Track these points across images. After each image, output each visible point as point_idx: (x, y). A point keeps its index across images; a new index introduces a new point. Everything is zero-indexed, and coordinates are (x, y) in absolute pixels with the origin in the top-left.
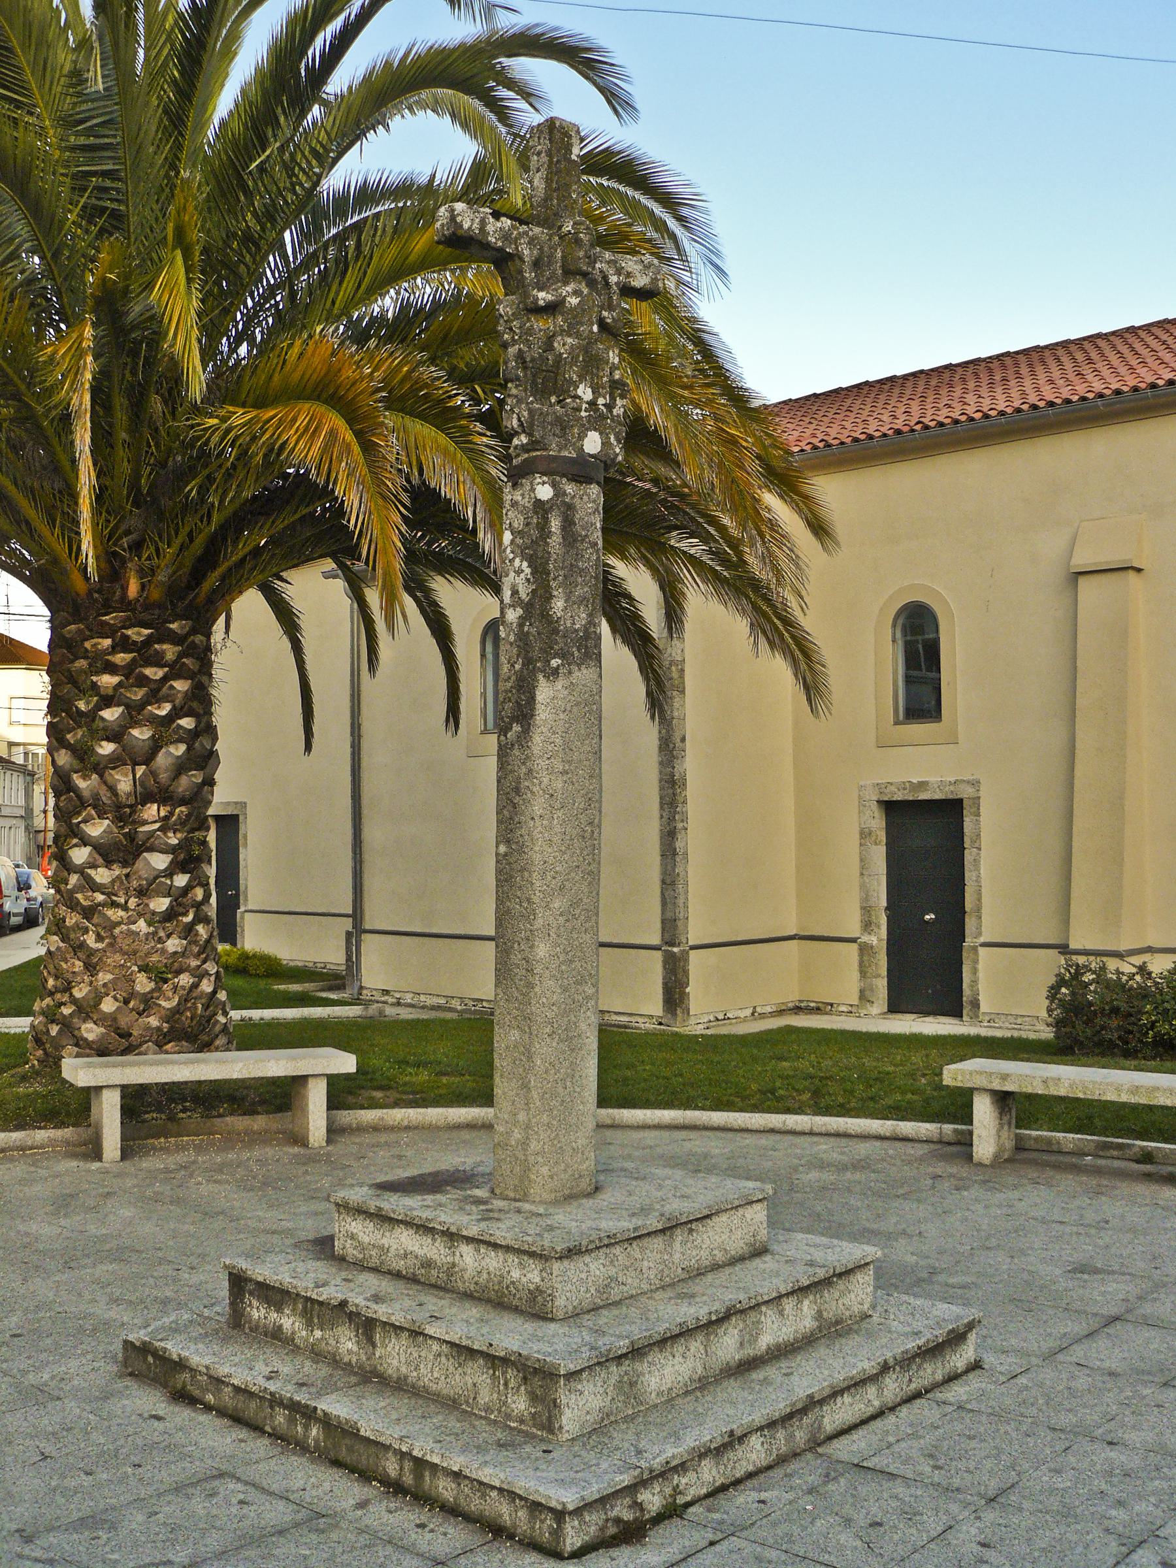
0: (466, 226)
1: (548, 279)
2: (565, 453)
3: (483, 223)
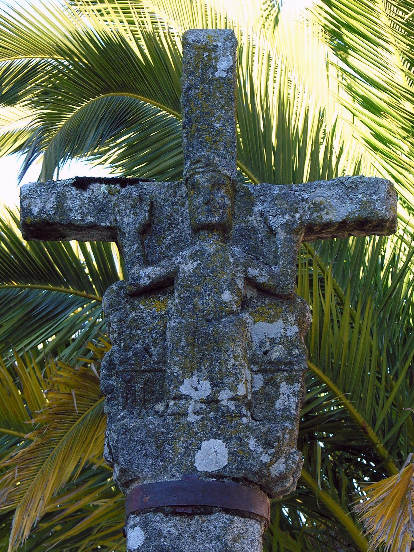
0: (35, 210)
1: (169, 248)
2: (167, 478)
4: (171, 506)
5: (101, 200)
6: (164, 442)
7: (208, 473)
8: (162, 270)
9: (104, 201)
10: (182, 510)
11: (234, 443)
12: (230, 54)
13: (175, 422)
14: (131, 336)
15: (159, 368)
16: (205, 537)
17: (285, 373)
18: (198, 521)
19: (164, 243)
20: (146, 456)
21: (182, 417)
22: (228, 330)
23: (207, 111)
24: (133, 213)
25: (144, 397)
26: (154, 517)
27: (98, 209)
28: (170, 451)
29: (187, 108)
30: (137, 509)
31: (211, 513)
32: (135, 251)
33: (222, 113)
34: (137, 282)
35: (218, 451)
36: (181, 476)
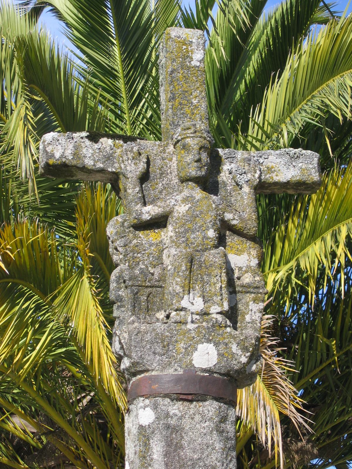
0: (57, 155)
1: (161, 192)
2: (171, 371)
3: (77, 148)
4: (177, 394)
5: (108, 151)
6: (169, 343)
7: (203, 369)
8: (160, 209)
9: (111, 152)
10: (184, 397)
11: (222, 347)
12: (202, 49)
13: (177, 328)
14: (134, 258)
15: (159, 286)
16: (201, 419)
17: (253, 295)
18: (196, 406)
19: (157, 188)
20: (154, 353)
21: (183, 325)
22: (217, 260)
23: (186, 90)
24: (134, 163)
25: (148, 306)
26: (162, 401)
27: (106, 158)
28: (174, 351)
29: (172, 87)
30: (146, 394)
31: (205, 400)
32: (138, 193)
33: (197, 93)
34: (140, 217)
35: (210, 352)
36: (182, 370)
